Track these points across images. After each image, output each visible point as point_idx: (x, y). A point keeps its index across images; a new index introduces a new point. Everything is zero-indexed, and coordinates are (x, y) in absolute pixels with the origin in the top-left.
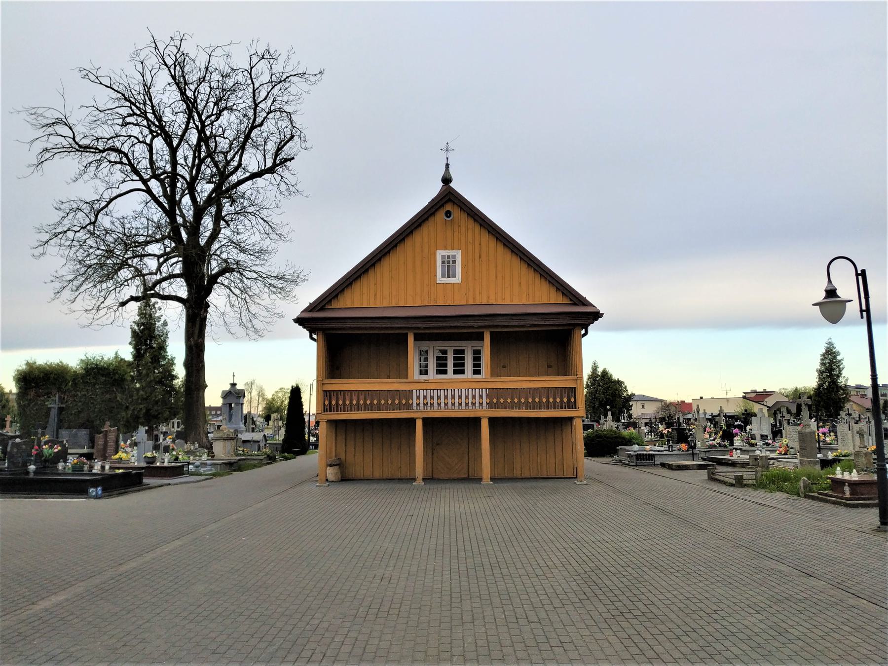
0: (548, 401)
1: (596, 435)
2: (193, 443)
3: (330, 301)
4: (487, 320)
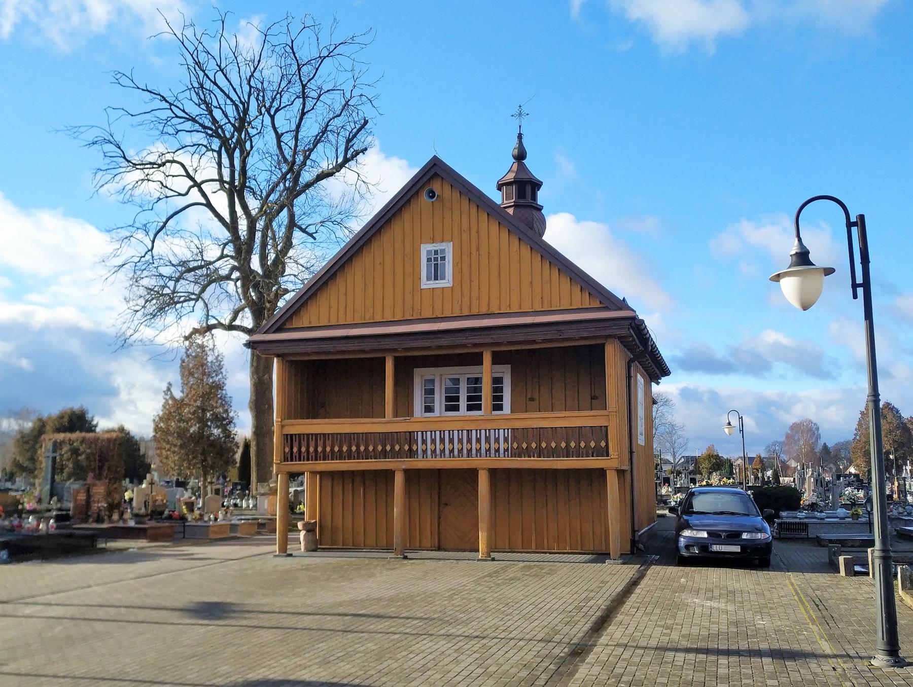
0: (568, 446)
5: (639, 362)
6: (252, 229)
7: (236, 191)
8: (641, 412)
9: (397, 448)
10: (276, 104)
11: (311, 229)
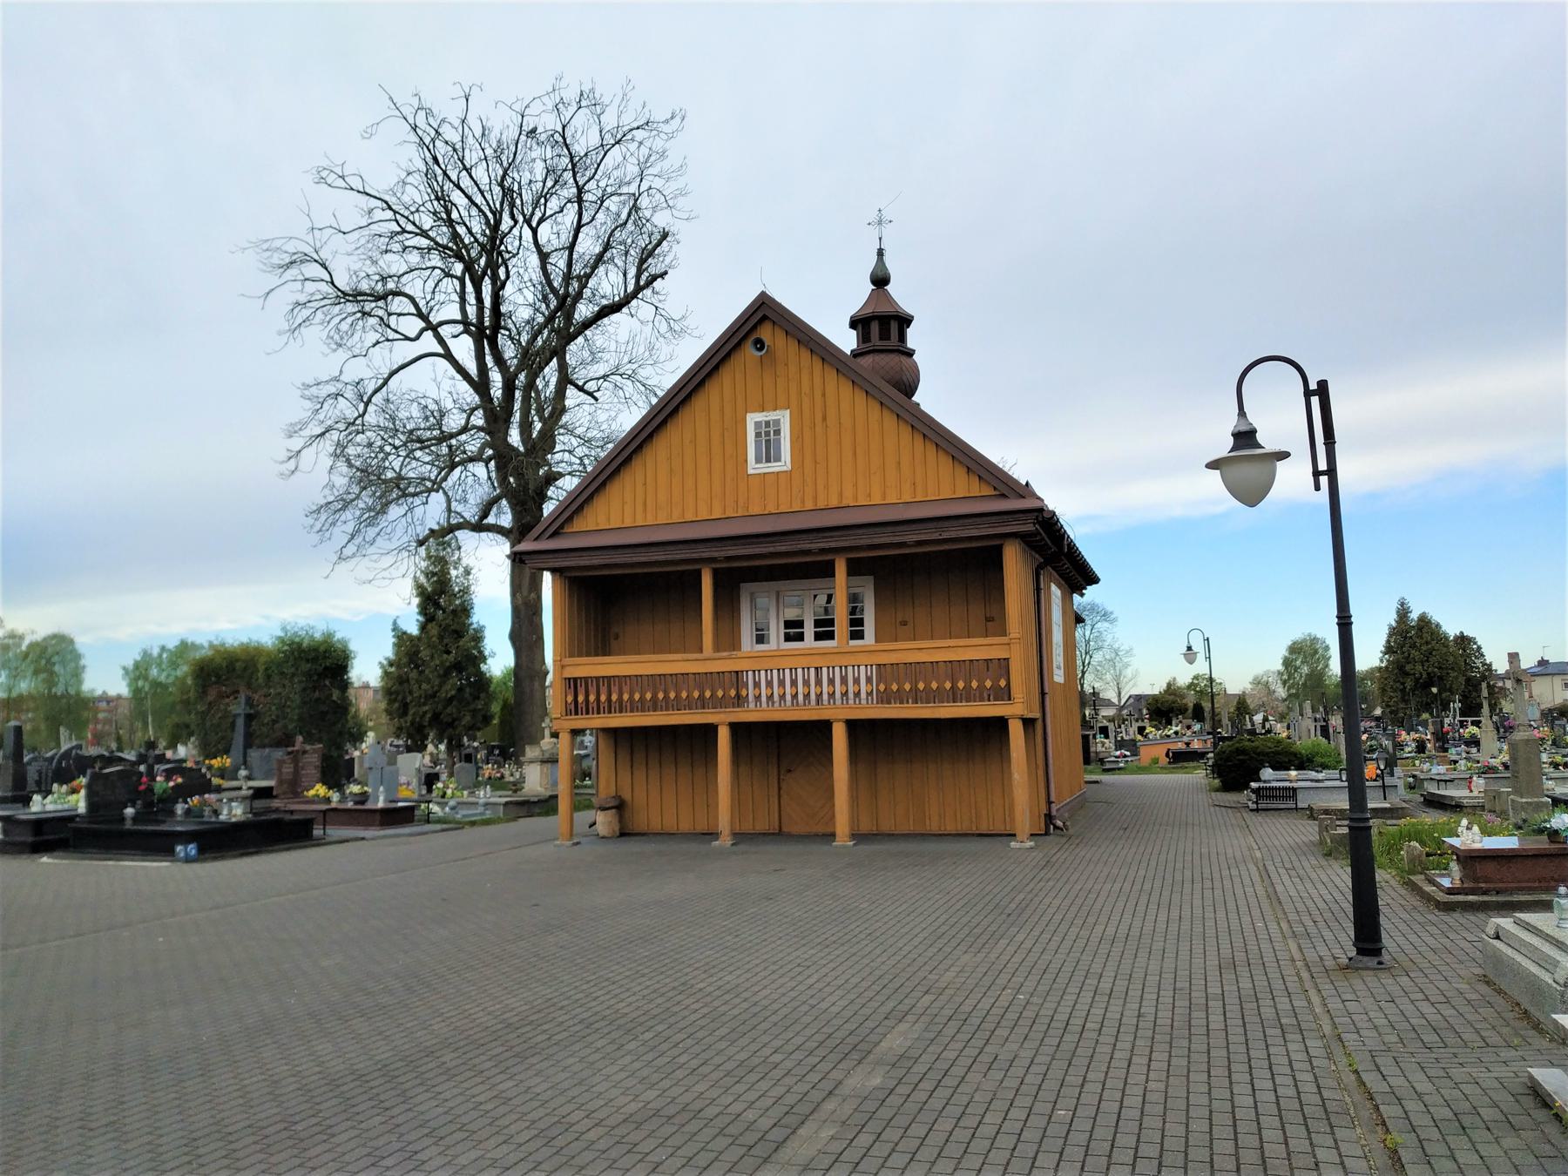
1: (1237, 749)
2: (205, 775)
4: (849, 535)
5: (1054, 568)
6: (509, 388)
7: (487, 337)
8: (1057, 636)
9: (720, 693)
10: (538, 214)
11: (591, 386)
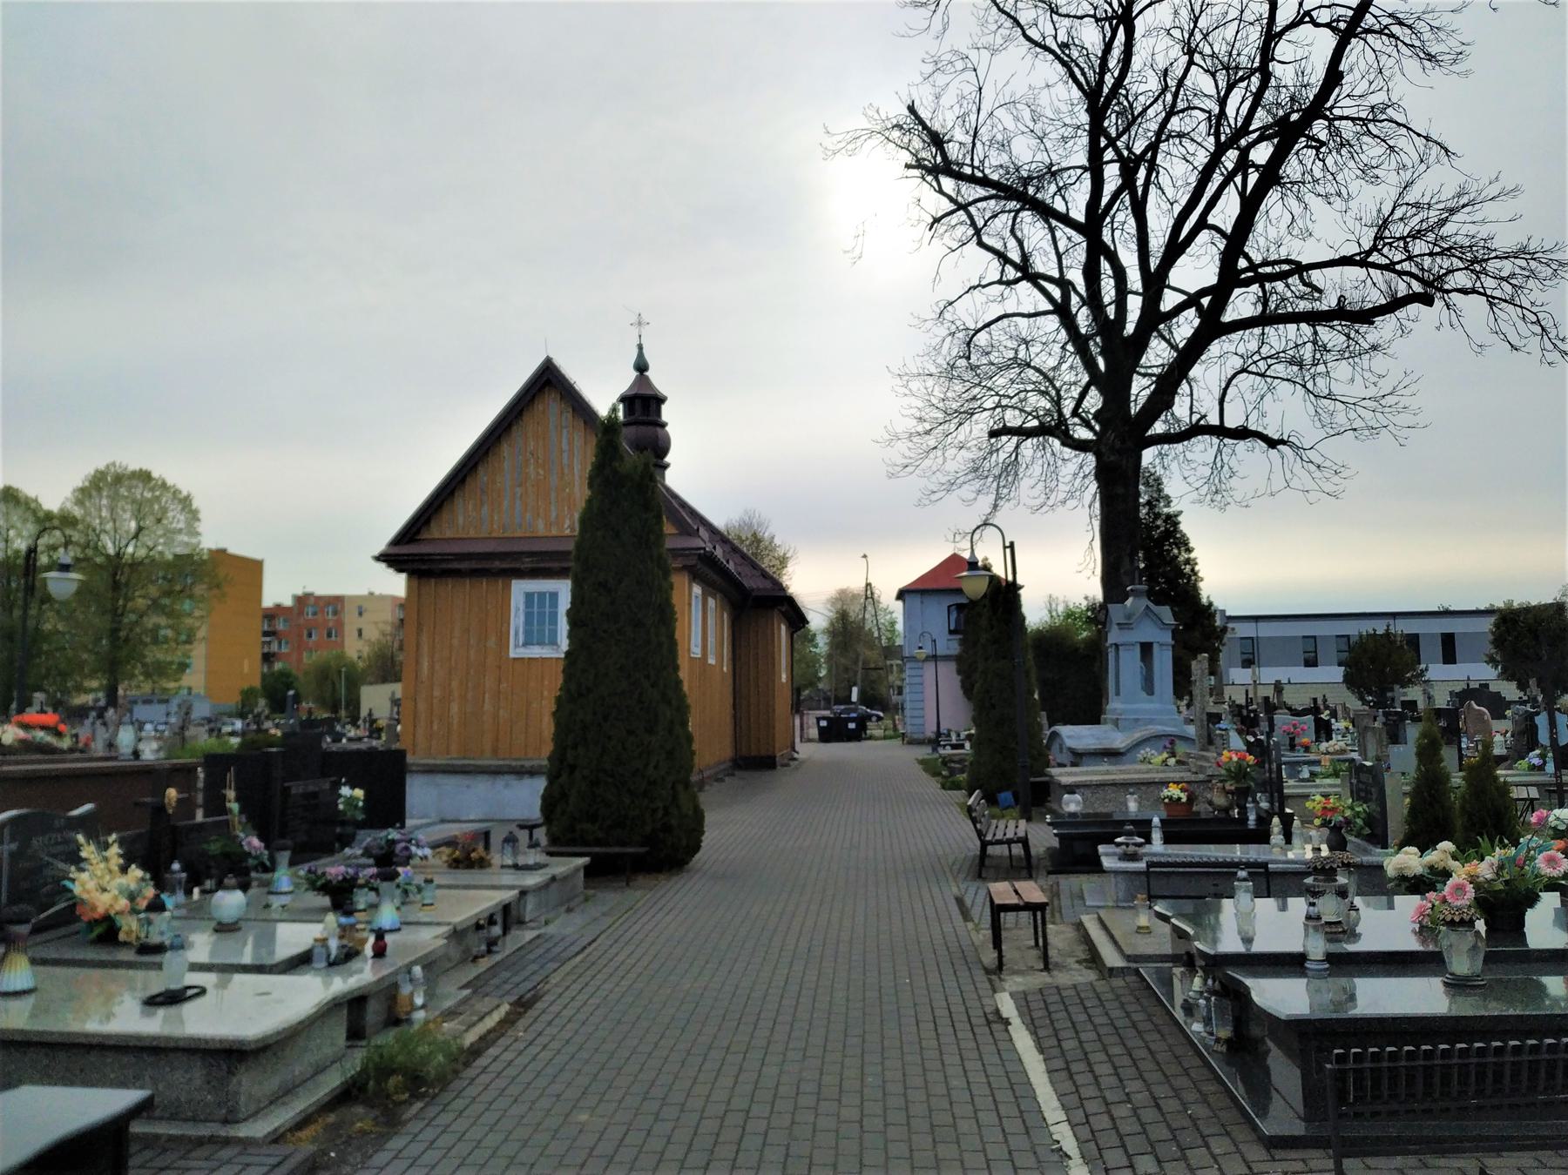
3: (418, 532)
